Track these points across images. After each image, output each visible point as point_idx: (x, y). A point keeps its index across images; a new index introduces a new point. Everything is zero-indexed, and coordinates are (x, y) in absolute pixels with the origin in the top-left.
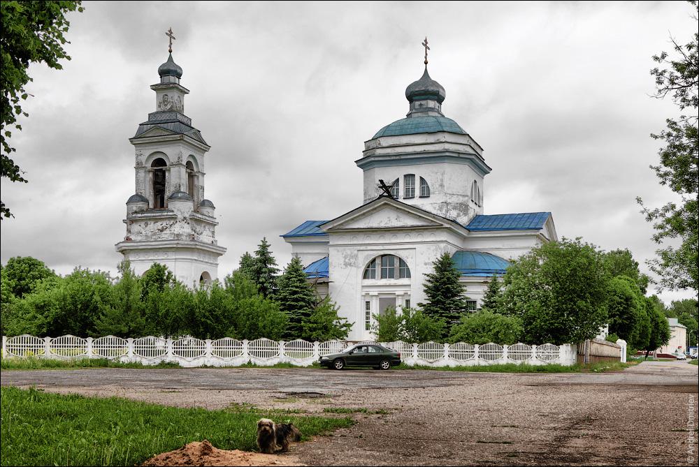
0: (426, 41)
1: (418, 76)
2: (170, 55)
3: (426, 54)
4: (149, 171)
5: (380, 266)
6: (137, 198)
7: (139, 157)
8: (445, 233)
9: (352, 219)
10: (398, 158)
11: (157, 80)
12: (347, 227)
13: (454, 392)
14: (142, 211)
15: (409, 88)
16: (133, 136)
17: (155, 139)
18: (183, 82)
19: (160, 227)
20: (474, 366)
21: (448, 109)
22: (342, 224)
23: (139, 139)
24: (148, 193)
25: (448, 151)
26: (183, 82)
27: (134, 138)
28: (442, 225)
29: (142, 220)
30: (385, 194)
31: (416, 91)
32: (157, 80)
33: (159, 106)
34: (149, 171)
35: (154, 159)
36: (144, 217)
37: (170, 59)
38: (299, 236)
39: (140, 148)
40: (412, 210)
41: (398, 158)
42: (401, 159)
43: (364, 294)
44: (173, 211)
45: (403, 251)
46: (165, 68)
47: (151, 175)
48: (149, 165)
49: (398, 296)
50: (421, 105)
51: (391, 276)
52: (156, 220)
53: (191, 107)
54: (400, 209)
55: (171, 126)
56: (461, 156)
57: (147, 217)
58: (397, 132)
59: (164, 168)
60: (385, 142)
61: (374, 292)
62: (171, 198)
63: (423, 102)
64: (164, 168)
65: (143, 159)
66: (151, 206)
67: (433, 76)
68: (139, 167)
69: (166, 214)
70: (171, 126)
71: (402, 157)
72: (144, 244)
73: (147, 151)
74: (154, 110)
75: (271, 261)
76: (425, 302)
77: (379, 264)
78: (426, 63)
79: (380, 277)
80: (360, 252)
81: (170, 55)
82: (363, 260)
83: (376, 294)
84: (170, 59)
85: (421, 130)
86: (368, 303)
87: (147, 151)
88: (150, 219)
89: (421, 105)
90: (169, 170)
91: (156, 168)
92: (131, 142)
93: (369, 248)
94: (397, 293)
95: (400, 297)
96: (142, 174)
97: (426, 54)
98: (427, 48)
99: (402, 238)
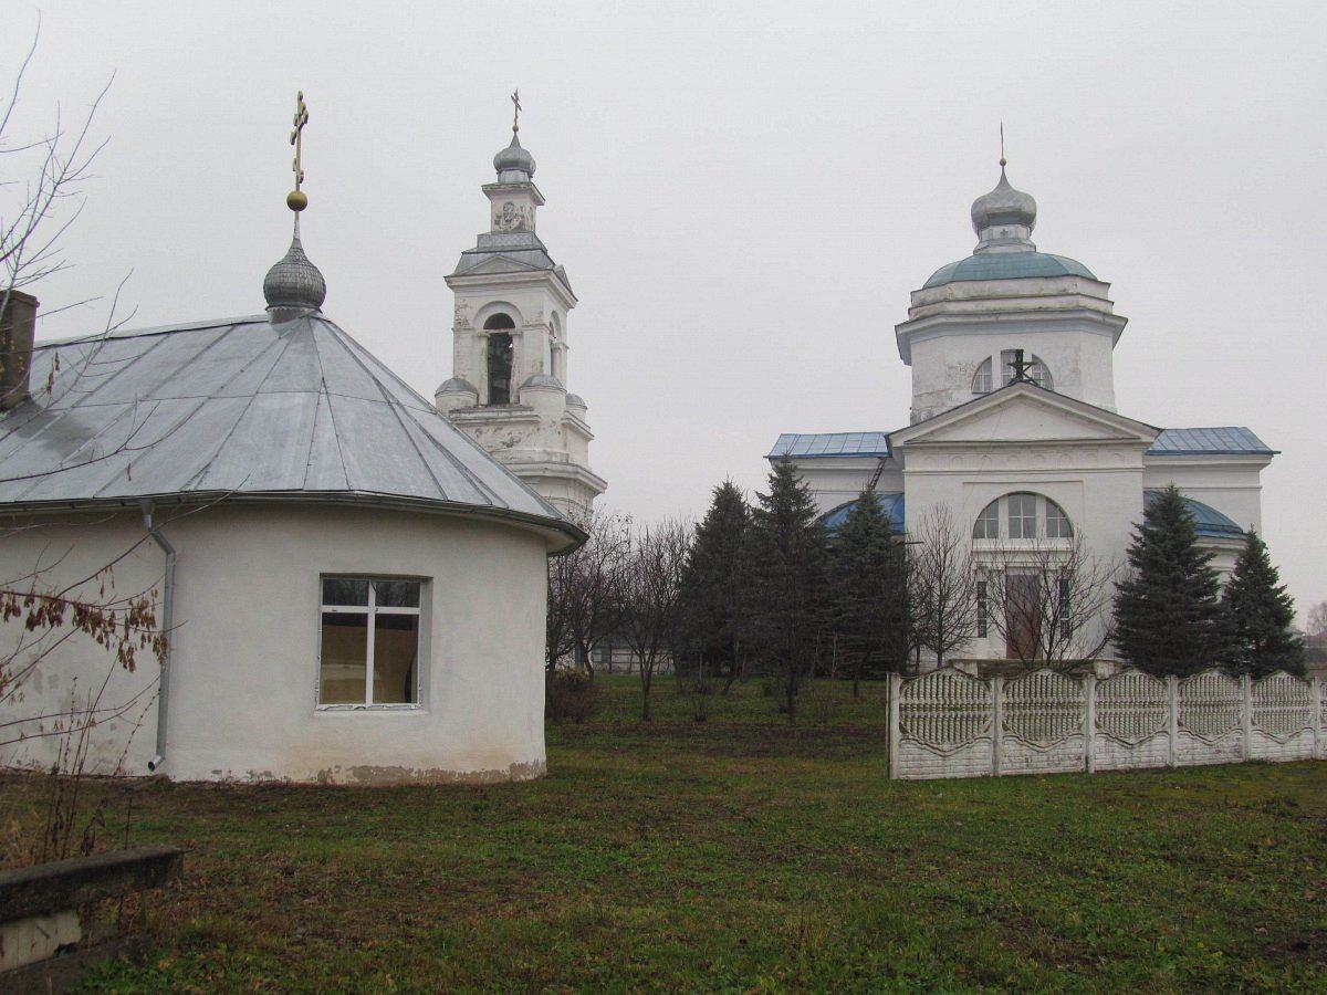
0: (516, 94)
1: (990, 185)
2: (516, 136)
3: (517, 117)
4: (480, 337)
6: (460, 384)
7: (463, 311)
9: (953, 424)
10: (993, 319)
11: (492, 177)
12: (942, 439)
14: (469, 410)
15: (975, 205)
16: (451, 271)
17: (496, 279)
19: (507, 440)
20: (1224, 673)
21: (1046, 239)
22: (932, 433)
23: (461, 280)
24: (478, 375)
25: (1084, 309)
27: (451, 276)
29: (471, 425)
31: (997, 209)
32: (492, 177)
33: (497, 223)
34: (480, 337)
35: (487, 317)
36: (475, 419)
37: (515, 141)
38: (404, 410)
39: (465, 295)
40: (1101, 417)
41: (993, 319)
42: (998, 322)
44: (531, 409)
45: (1053, 486)
46: (502, 157)
47: (484, 344)
48: (480, 326)
50: (1004, 233)
52: (499, 425)
53: (550, 226)
54: (1097, 422)
55: (525, 256)
56: (1002, 318)
57: (480, 418)
58: (979, 275)
59: (511, 332)
60: (958, 290)
62: (528, 385)
63: (1009, 228)
64: (511, 332)
65: (469, 314)
66: (484, 399)
67: (1016, 183)
68: (460, 327)
69: (519, 413)
70: (525, 256)
71: (1002, 318)
72: (523, 467)
73: (478, 300)
74: (487, 229)
75: (799, 497)
78: (516, 129)
81: (516, 136)
84: (515, 141)
85: (1024, 273)
87: (478, 300)
88: (487, 422)
90: (520, 336)
91: (492, 331)
92: (448, 282)
96: (467, 339)
97: (517, 117)
98: (518, 106)
99: (1051, 462)
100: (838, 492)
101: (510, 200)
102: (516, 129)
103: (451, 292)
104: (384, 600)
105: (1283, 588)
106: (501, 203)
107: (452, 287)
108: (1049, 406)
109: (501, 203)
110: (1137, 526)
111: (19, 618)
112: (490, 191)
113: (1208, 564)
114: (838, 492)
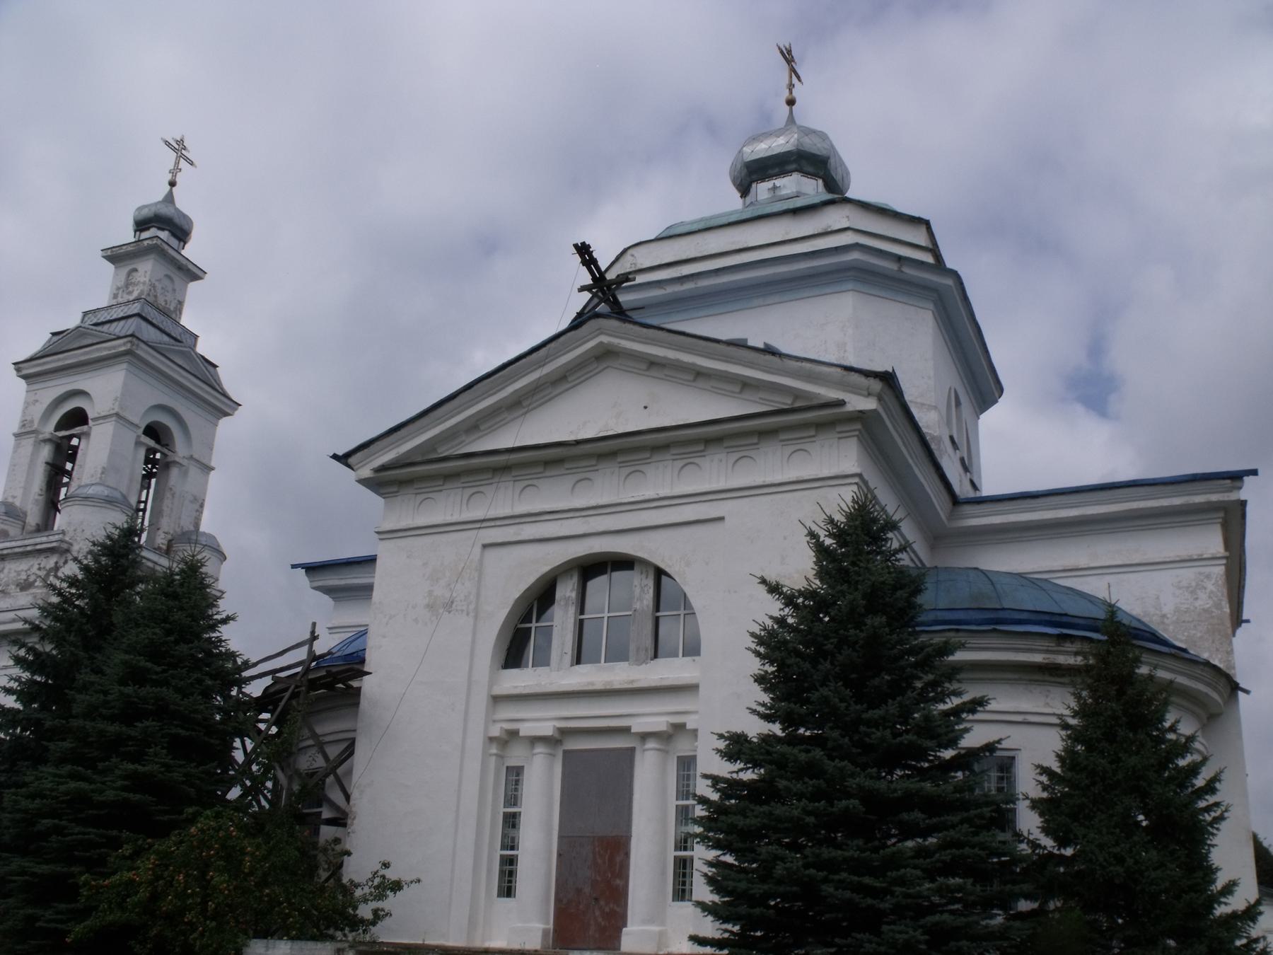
2: (171, 190)
5: (572, 610)
8: (850, 286)
11: (126, 235)
13: (803, 364)
18: (192, 251)
22: (173, 345)
26: (192, 251)
28: (841, 403)
30: (603, 308)
33: (115, 296)
34: (45, 441)
37: (169, 198)
40: (728, 359)
43: (495, 731)
49: (644, 737)
50: (775, 188)
51: (618, 654)
61: (541, 721)
73: (52, 390)
76: (755, 728)
77: (567, 599)
78: (172, 184)
79: (568, 658)
80: (492, 554)
81: (171, 190)
82: (165, 273)
83: (547, 729)
84: (169, 198)
86: (515, 774)
87: (52, 390)
89: (775, 188)
92: (18, 370)
93: (529, 531)
94: (638, 726)
95: (651, 744)
96: (28, 443)
100: (351, 632)
101: (172, 275)
102: (172, 184)
103: (22, 382)
104: (683, 872)
105: (759, 669)
106: (124, 271)
107: (25, 377)
108: (1182, 706)
109: (124, 271)
110: (771, 617)
111: (385, 874)
112: (116, 256)
113: (1058, 770)
114: (351, 632)
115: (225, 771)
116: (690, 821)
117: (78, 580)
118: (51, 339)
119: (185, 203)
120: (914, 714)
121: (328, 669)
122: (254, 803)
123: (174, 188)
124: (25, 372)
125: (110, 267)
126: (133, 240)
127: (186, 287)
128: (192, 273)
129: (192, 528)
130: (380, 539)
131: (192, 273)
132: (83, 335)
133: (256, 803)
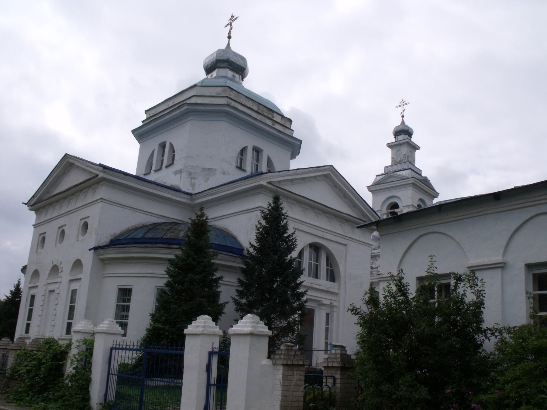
11: (392, 139)
37: (403, 122)
84: (403, 122)
102: (403, 117)
115: (465, 322)
116: (480, 310)
117: (327, 359)
118: (376, 179)
119: (409, 123)
120: (247, 304)
121: (332, 302)
122: (248, 255)
123: (404, 118)
124: (371, 189)
125: (390, 150)
126: (395, 141)
127: (415, 152)
128: (415, 148)
129: (354, 314)
130: (215, 378)
131: (415, 148)
132: (376, 248)
133: (247, 256)
